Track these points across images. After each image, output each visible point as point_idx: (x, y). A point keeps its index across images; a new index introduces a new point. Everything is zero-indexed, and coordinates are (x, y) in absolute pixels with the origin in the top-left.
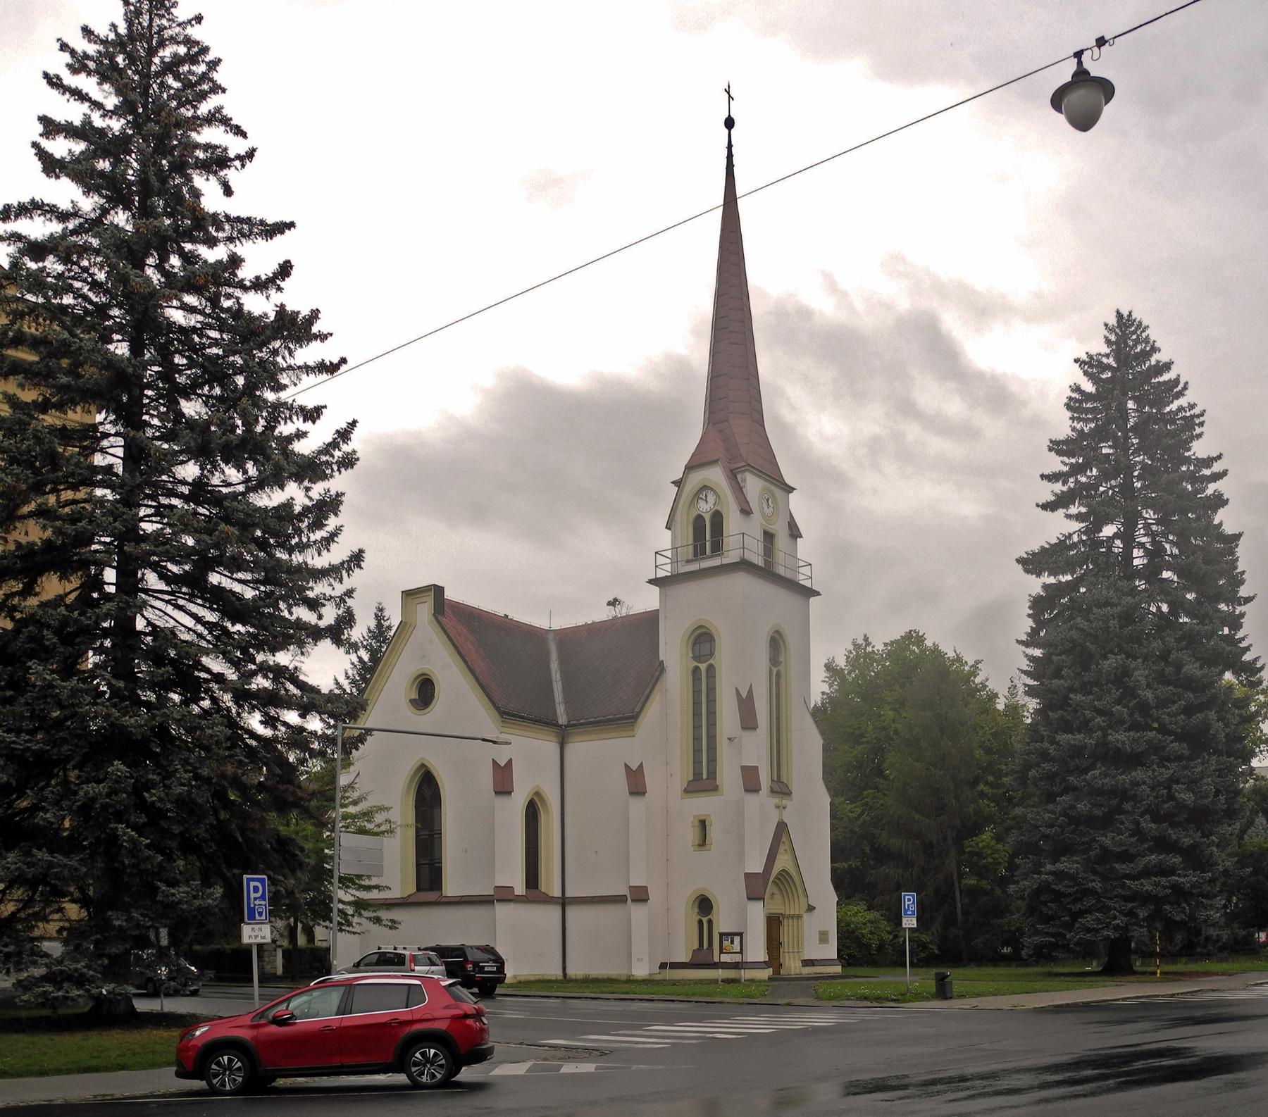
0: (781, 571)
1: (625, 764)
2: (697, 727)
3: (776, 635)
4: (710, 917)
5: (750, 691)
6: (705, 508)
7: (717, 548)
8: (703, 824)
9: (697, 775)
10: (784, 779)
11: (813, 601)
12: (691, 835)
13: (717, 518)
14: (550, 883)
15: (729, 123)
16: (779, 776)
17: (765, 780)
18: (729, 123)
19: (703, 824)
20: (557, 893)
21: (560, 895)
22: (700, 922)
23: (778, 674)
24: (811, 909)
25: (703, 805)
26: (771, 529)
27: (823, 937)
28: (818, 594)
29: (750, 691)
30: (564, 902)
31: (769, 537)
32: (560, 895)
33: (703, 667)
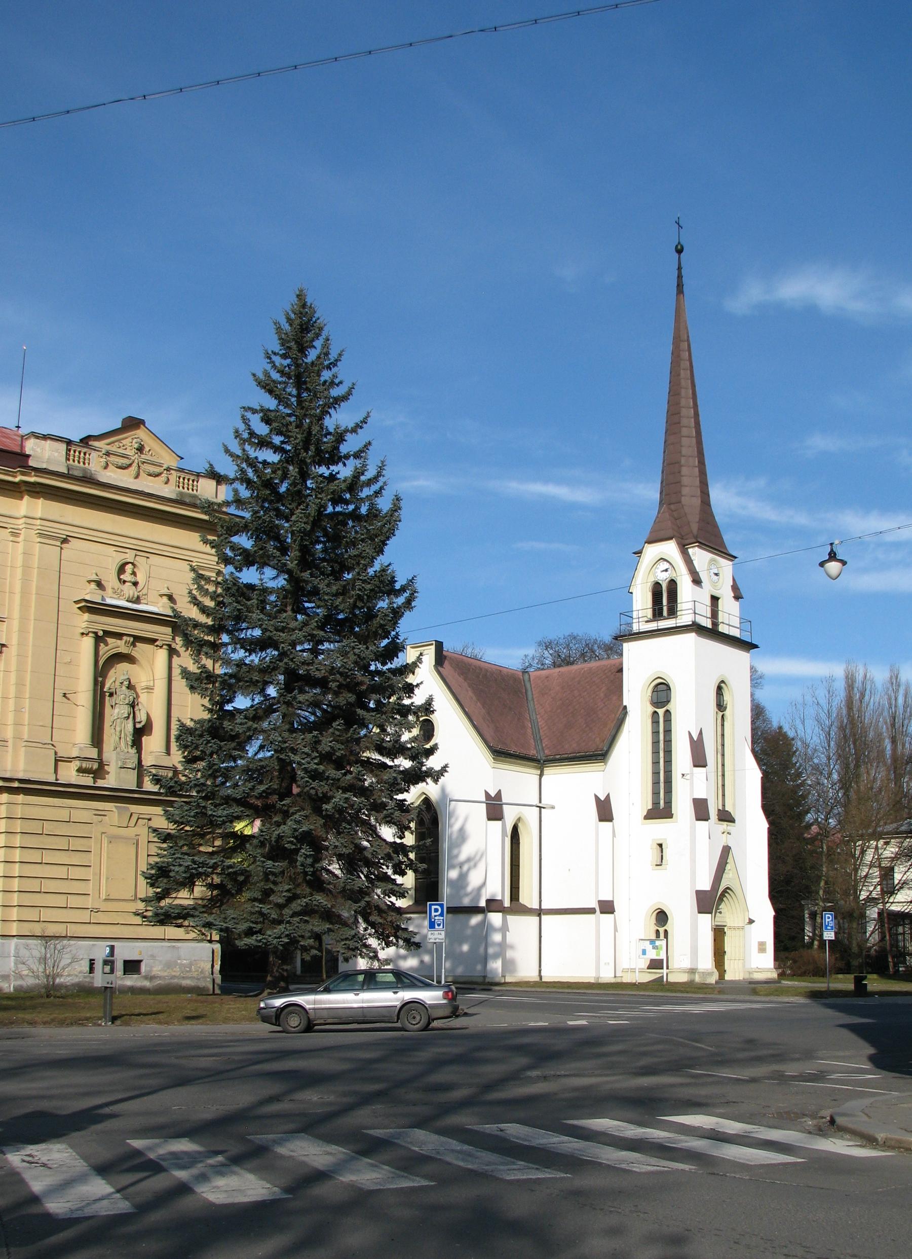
0: (722, 629)
1: (609, 795)
2: (656, 763)
4: (665, 928)
5: (701, 733)
6: (663, 578)
7: (673, 612)
8: (660, 845)
9: (656, 803)
12: (652, 855)
13: (673, 584)
14: (528, 898)
15: (679, 251)
16: (724, 805)
18: (679, 251)
19: (660, 845)
20: (535, 906)
21: (538, 907)
22: (658, 931)
24: (751, 922)
25: (660, 828)
26: (716, 594)
27: (762, 947)
29: (701, 733)
30: (540, 912)
31: (715, 599)
32: (538, 907)
33: (661, 712)
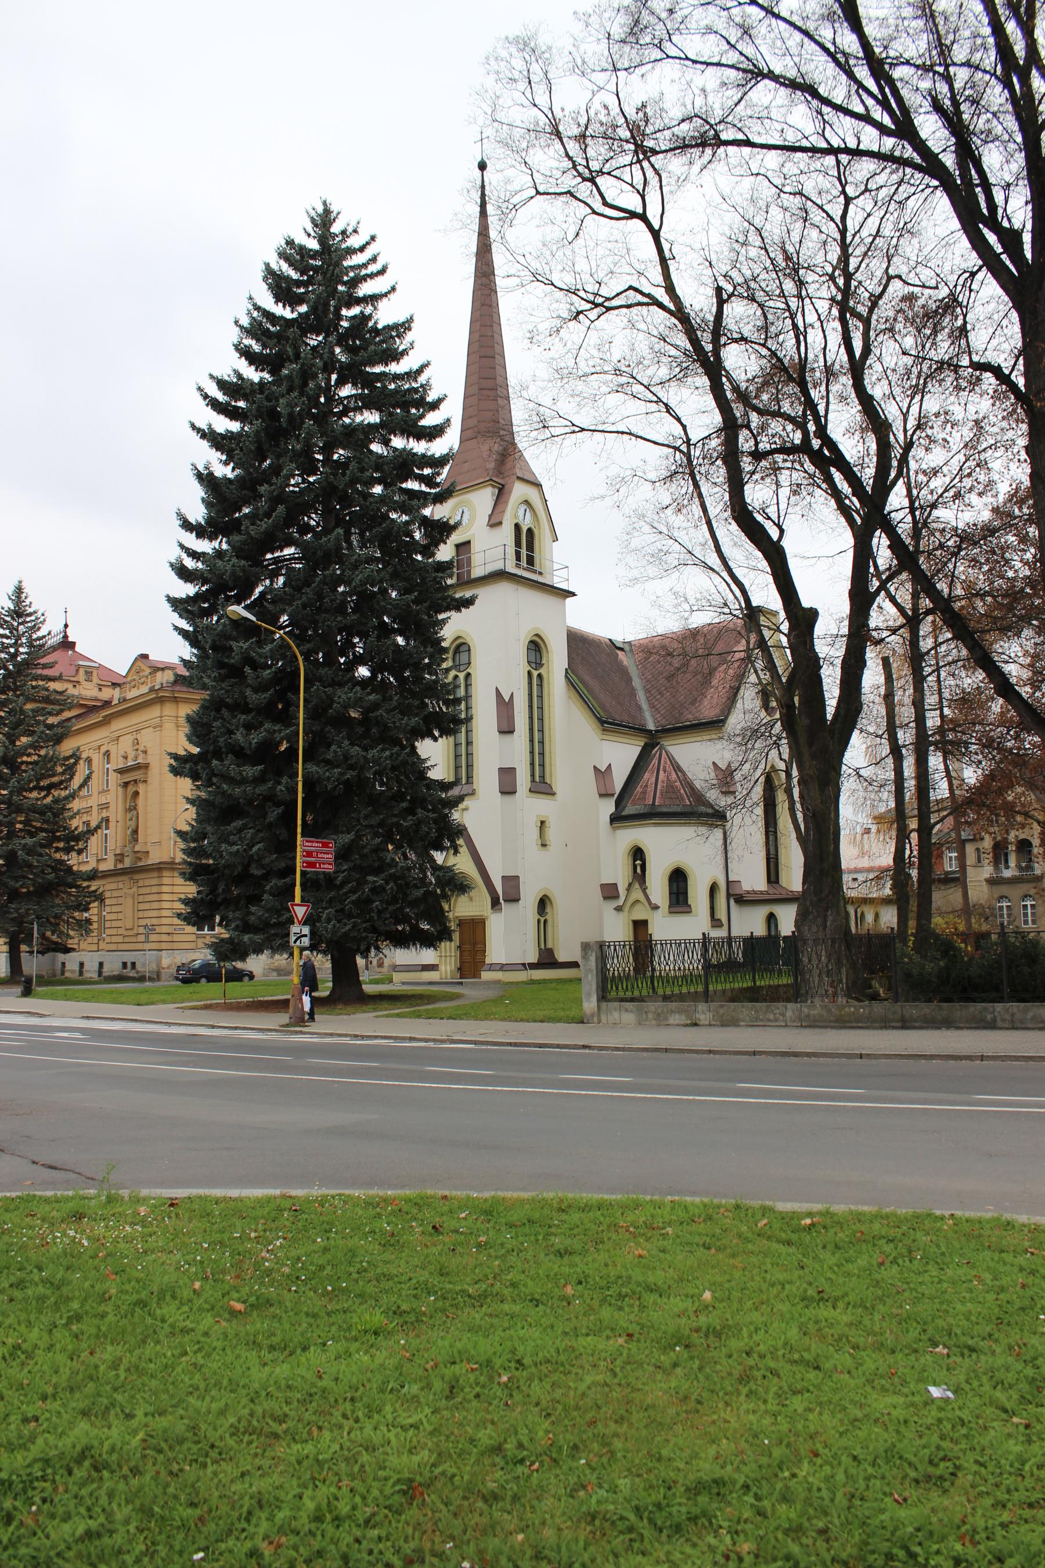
2: (541, 708)
3: (536, 639)
10: (548, 780)
11: (569, 601)
15: (482, 166)
16: (542, 777)
17: (523, 780)
18: (482, 166)
23: (540, 676)
28: (573, 594)
